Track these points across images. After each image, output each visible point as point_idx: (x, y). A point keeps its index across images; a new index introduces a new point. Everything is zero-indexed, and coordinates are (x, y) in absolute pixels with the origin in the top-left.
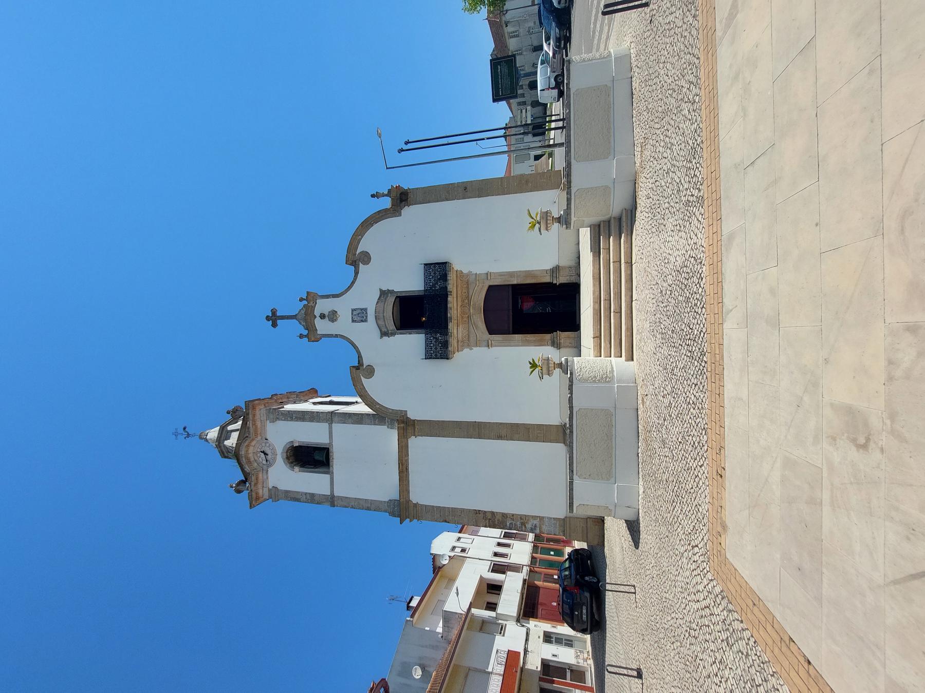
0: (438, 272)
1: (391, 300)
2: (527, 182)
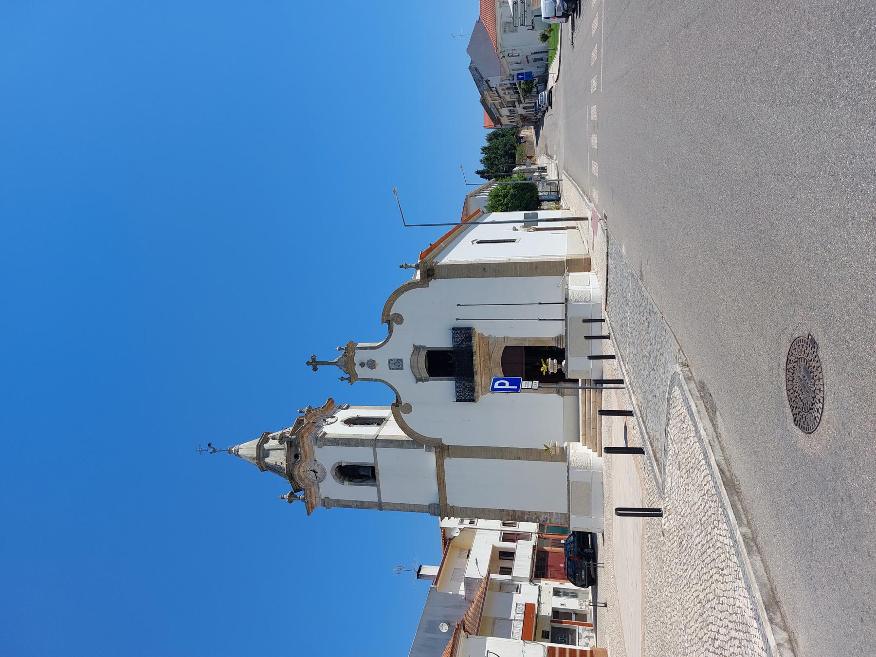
0: (464, 335)
1: (423, 354)
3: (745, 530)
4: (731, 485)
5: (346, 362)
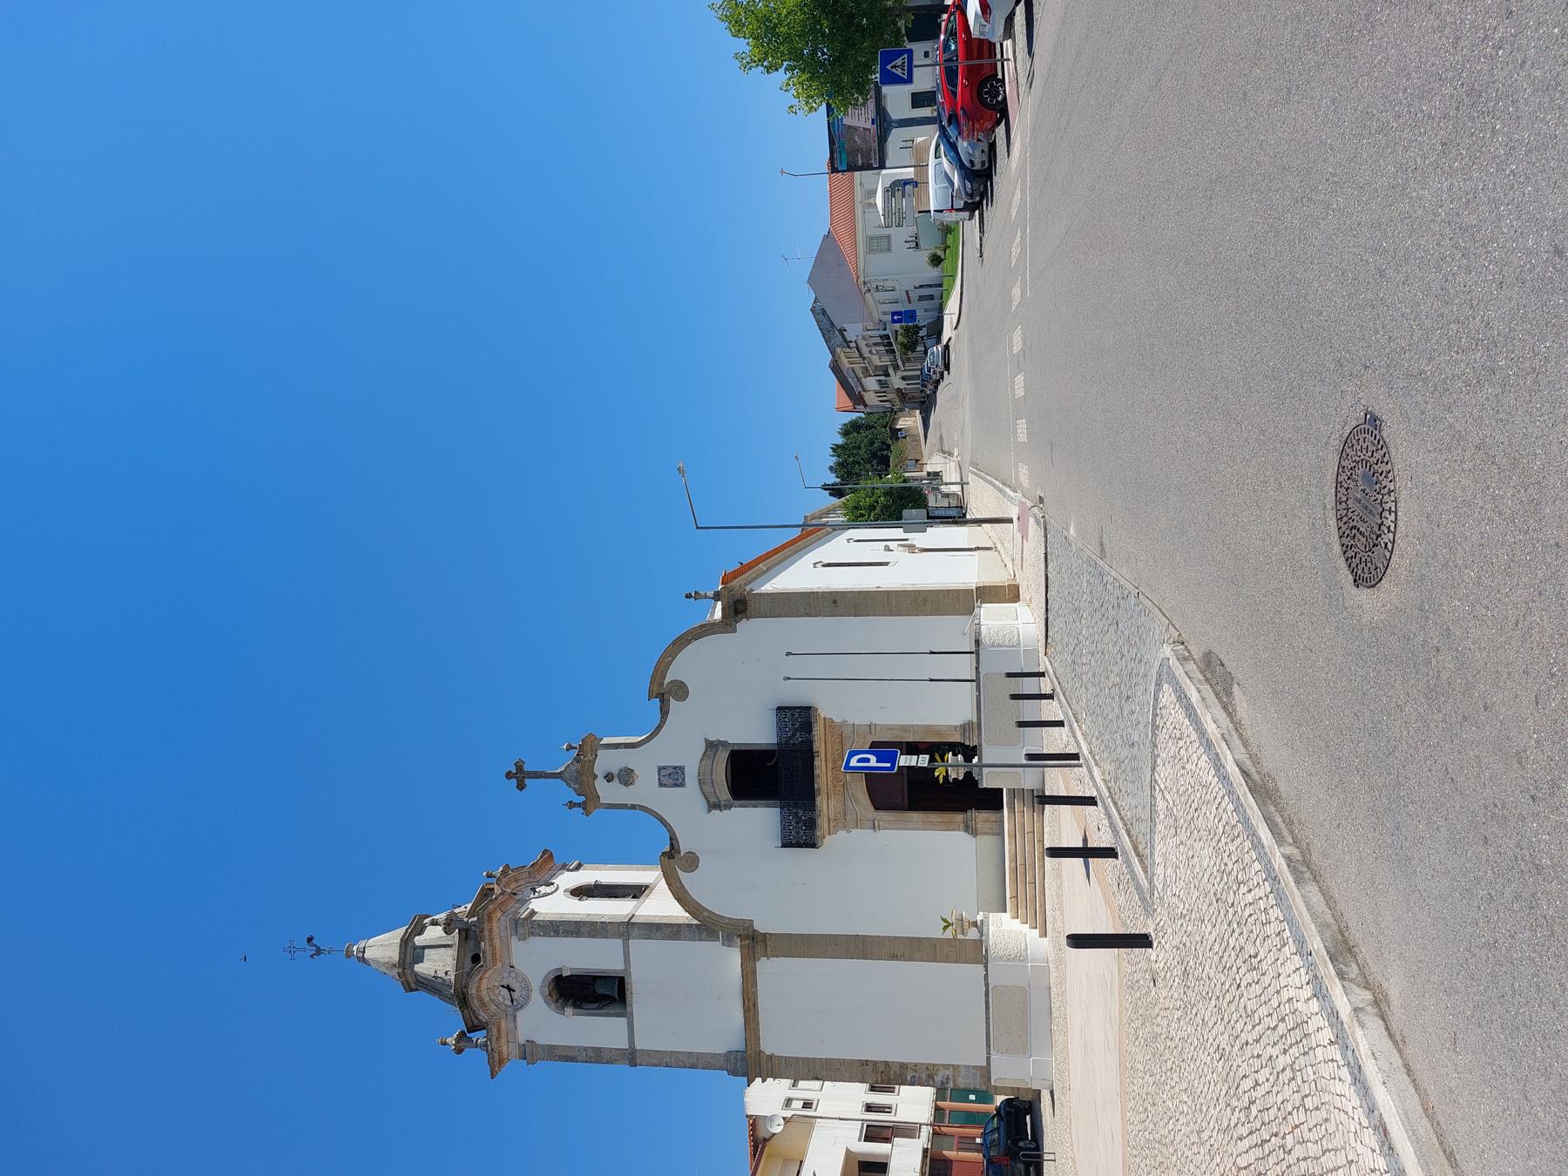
1: (723, 756)
2: (925, 600)
3: (1290, 850)
4: (1263, 791)
5: (580, 773)
